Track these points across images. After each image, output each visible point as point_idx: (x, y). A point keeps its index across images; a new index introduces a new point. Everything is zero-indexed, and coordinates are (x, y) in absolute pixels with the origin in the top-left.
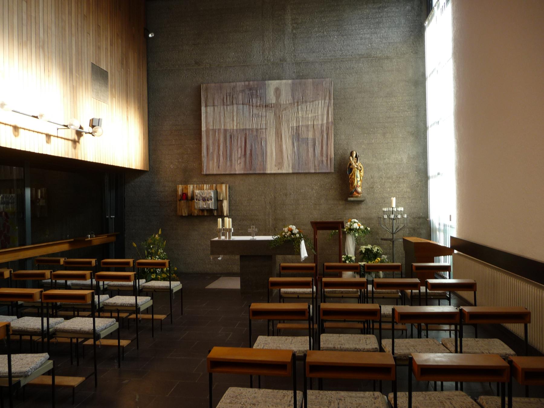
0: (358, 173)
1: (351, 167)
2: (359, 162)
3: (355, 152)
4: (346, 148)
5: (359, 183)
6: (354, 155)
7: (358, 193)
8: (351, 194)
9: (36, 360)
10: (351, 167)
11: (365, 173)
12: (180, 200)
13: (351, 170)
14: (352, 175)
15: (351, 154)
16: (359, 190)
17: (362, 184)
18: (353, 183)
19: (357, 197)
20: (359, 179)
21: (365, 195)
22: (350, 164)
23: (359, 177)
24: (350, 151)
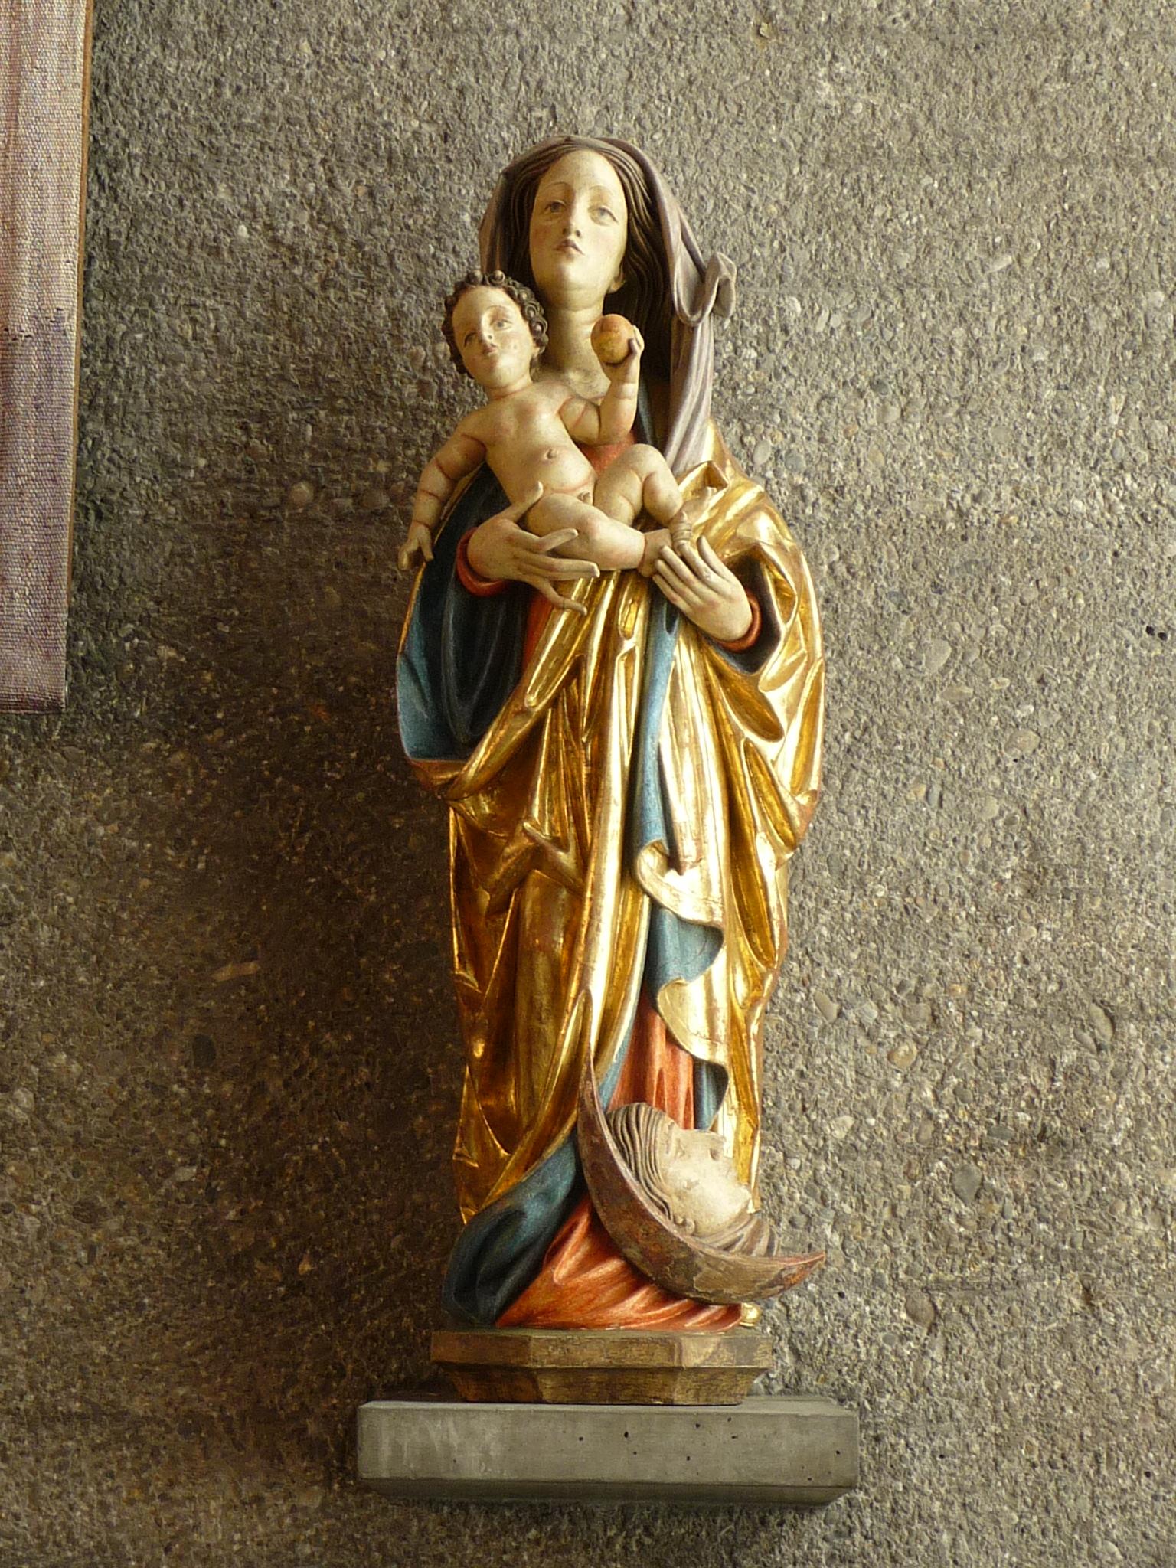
0: (673, 728)
1: (493, 545)
2: (701, 435)
3: (598, 178)
4: (407, 126)
5: (702, 1007)
6: (592, 260)
7: (664, 1270)
8: (465, 1311)
9: (680, 1434)
10: (493, 545)
11: (858, 743)
12: (305, 1542)
13: (490, 628)
14: (513, 777)
15: (519, 231)
16: (703, 1178)
17: (789, 1028)
18: (514, 1013)
19: (623, 1383)
20: (694, 892)
21: (870, 1321)
22: (482, 488)
23: (692, 862)
24: (505, 145)
